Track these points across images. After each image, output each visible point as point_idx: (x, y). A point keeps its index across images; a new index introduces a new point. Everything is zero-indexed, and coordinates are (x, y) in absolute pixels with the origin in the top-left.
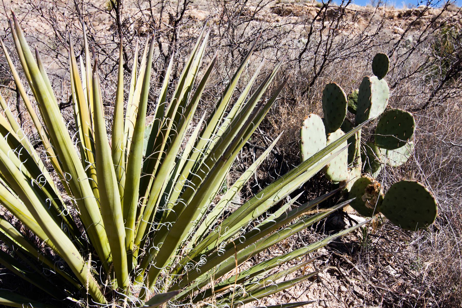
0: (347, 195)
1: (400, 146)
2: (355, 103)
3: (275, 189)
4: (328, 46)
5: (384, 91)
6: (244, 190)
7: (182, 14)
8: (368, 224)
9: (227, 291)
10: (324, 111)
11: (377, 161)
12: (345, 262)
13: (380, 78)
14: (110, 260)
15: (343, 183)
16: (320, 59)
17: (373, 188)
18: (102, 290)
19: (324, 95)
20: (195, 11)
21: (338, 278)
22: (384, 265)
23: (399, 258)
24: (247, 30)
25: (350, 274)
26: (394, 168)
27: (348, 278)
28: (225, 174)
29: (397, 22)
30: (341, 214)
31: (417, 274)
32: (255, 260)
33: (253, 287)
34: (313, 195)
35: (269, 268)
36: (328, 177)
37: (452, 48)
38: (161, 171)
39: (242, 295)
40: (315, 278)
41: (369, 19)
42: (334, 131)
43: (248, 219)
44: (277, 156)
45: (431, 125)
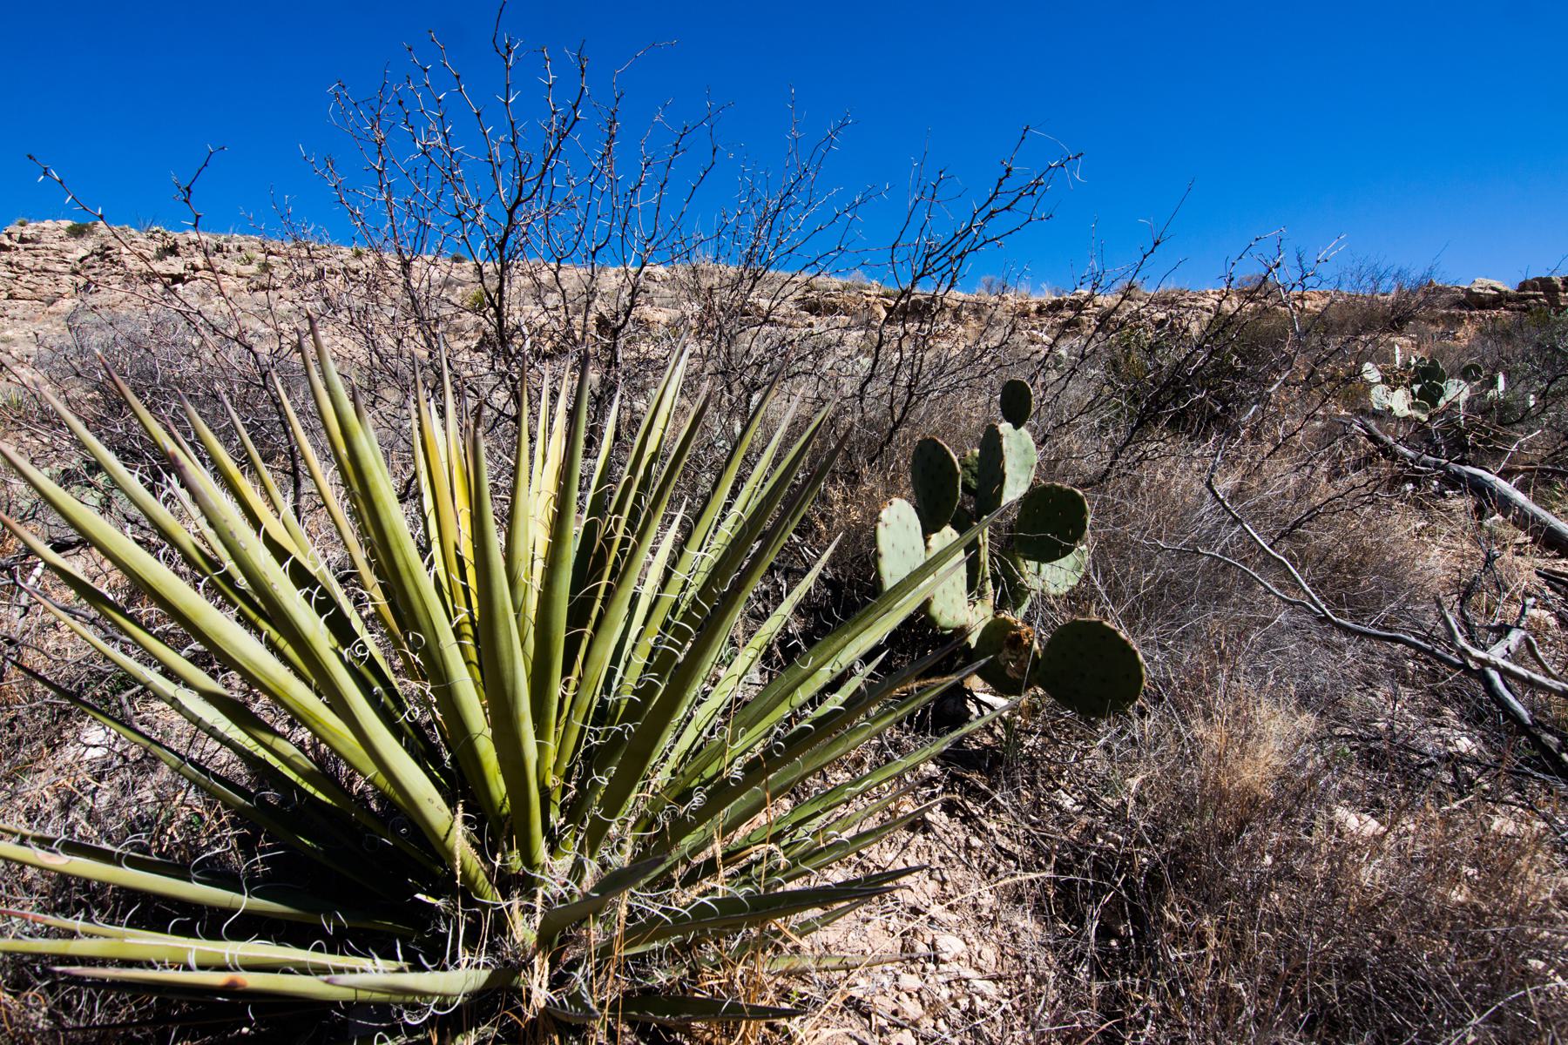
0: (970, 655)
1: (1064, 555)
2: (973, 475)
3: (835, 647)
4: (916, 370)
5: (1025, 451)
6: (767, 657)
7: (628, 314)
8: (1014, 710)
9: (744, 862)
10: (916, 492)
11: (1022, 586)
12: (976, 789)
13: (1017, 426)
14: (505, 811)
15: (962, 632)
16: (901, 394)
17: (1018, 638)
18: (489, 877)
19: (914, 461)
20: (647, 308)
21: (963, 821)
22: (1050, 790)
23: (1078, 772)
24: (753, 342)
25: (987, 811)
26: (1055, 597)
27: (983, 821)
28: (736, 619)
29: (1036, 323)
30: (960, 693)
31: (1115, 804)
32: (797, 796)
33: (799, 849)
34: (902, 659)
35: (830, 808)
36: (931, 621)
37: (1142, 367)
38: (607, 623)
39: (778, 866)
40: (918, 824)
41: (984, 318)
42: (938, 530)
43: (784, 711)
44: (829, 584)
45: (1116, 512)
